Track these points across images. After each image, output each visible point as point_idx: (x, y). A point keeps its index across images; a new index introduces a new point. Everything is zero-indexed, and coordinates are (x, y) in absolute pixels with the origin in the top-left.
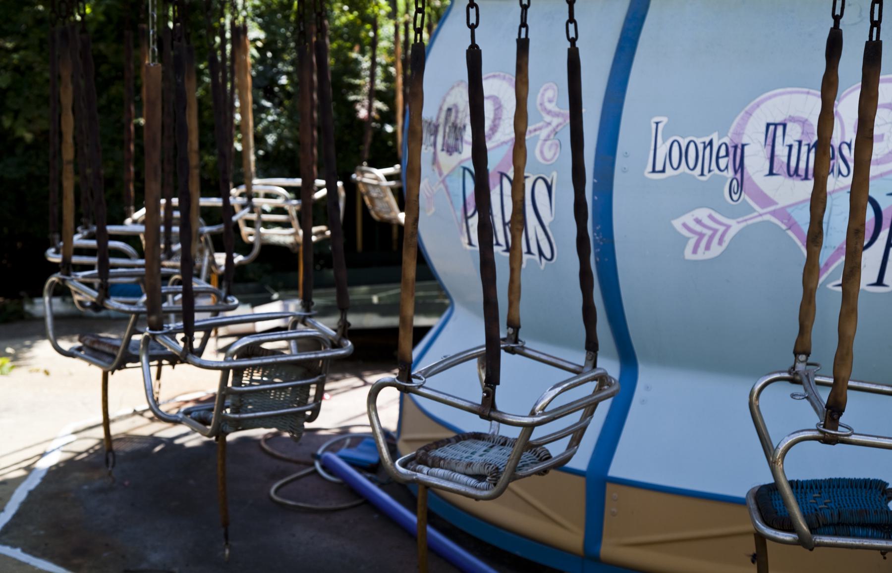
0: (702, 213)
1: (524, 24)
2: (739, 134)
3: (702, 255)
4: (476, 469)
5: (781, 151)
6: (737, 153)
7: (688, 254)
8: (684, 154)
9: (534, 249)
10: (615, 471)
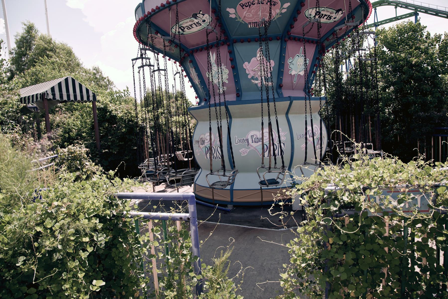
0: (243, 149)
1: (311, 117)
2: (247, 137)
3: (244, 155)
4: (222, 185)
5: (253, 139)
6: (247, 140)
7: (242, 155)
8: (240, 141)
9: (218, 157)
10: (234, 189)
